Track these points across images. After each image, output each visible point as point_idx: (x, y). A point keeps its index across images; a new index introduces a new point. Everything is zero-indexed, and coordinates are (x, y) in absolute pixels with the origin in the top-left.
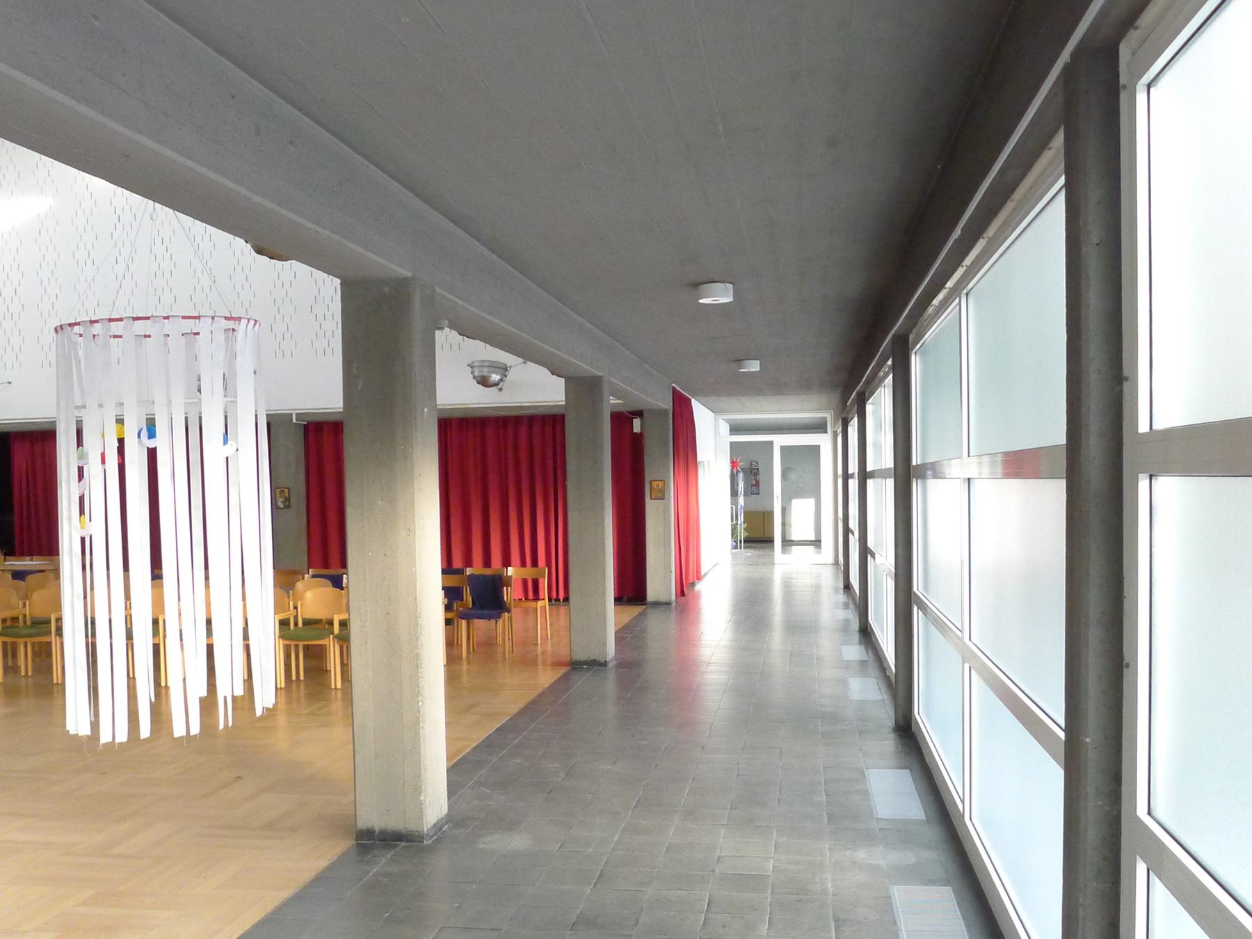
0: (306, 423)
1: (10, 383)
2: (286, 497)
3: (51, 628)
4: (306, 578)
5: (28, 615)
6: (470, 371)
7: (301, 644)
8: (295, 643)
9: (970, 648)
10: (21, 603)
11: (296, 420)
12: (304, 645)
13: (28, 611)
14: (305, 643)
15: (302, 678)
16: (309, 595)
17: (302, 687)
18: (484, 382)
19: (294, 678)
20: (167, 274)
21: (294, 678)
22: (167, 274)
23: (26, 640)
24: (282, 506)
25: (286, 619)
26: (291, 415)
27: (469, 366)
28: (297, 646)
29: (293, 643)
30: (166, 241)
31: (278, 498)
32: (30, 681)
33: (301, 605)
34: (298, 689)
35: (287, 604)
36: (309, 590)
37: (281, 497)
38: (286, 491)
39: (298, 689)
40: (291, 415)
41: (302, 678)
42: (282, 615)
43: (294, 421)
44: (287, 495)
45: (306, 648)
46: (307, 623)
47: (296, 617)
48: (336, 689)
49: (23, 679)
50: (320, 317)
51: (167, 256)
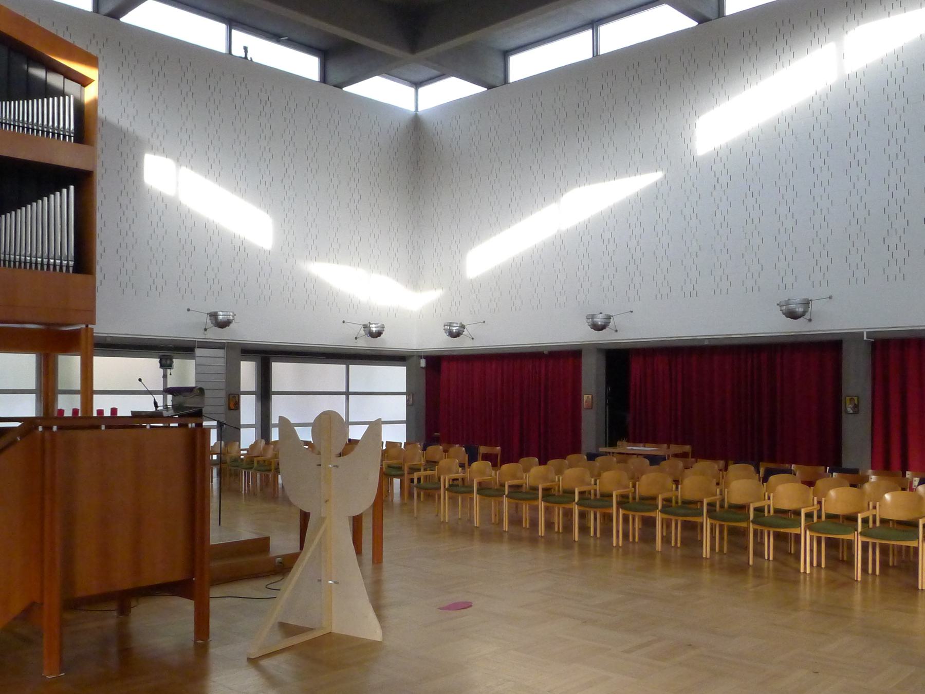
0: (873, 340)
1: (632, 312)
2: (855, 404)
3: (538, 494)
4: (834, 476)
5: (679, 497)
6: (779, 309)
7: (726, 524)
8: (761, 528)
9: (894, 540)
10: (593, 480)
11: (867, 338)
12: (728, 526)
13: (680, 493)
14: (685, 519)
15: (878, 572)
16: (832, 493)
17: (878, 580)
18: (793, 315)
19: (870, 571)
20: (756, 221)
21: (870, 571)
22: (756, 221)
23: (595, 510)
24: (851, 412)
25: (761, 507)
26: (863, 332)
27: (778, 305)
28: (874, 545)
29: (870, 540)
30: (756, 195)
31: (847, 405)
32: (679, 552)
33: (825, 501)
34: (874, 582)
35: (812, 499)
36: (831, 489)
37: (850, 403)
38: (856, 399)
39: (874, 582)
40: (863, 332)
41: (878, 572)
42: (619, 491)
43: (865, 338)
44: (856, 402)
45: (827, 539)
46: (830, 517)
47: (820, 511)
48: (857, 580)
49: (673, 550)
50: (892, 247)
51: (756, 206)
